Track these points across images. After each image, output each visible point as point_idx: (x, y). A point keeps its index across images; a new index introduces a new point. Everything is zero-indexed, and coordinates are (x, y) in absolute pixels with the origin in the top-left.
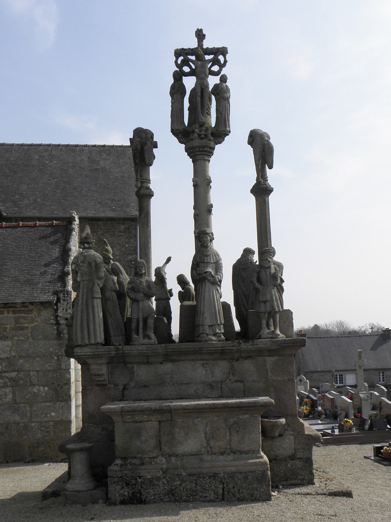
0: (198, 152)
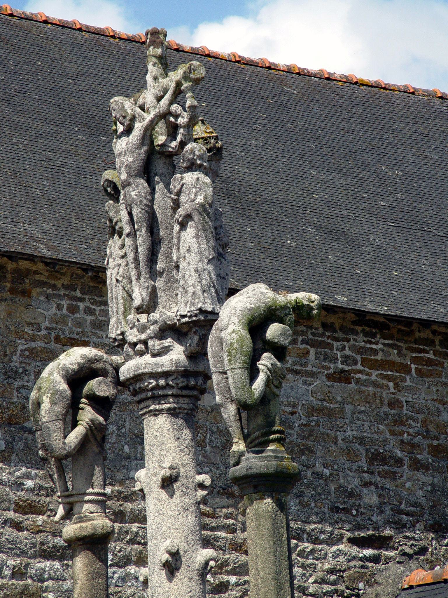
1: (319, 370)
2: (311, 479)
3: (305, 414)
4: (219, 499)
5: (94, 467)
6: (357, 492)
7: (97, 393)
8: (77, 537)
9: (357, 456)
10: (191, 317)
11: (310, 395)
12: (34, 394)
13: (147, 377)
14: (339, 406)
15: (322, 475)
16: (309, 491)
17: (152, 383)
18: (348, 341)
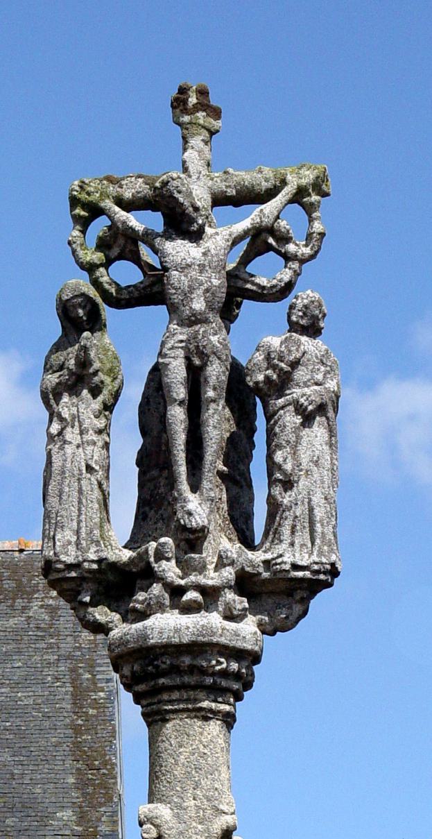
0: (164, 674)
10: (318, 572)
13: (216, 649)
17: (222, 663)
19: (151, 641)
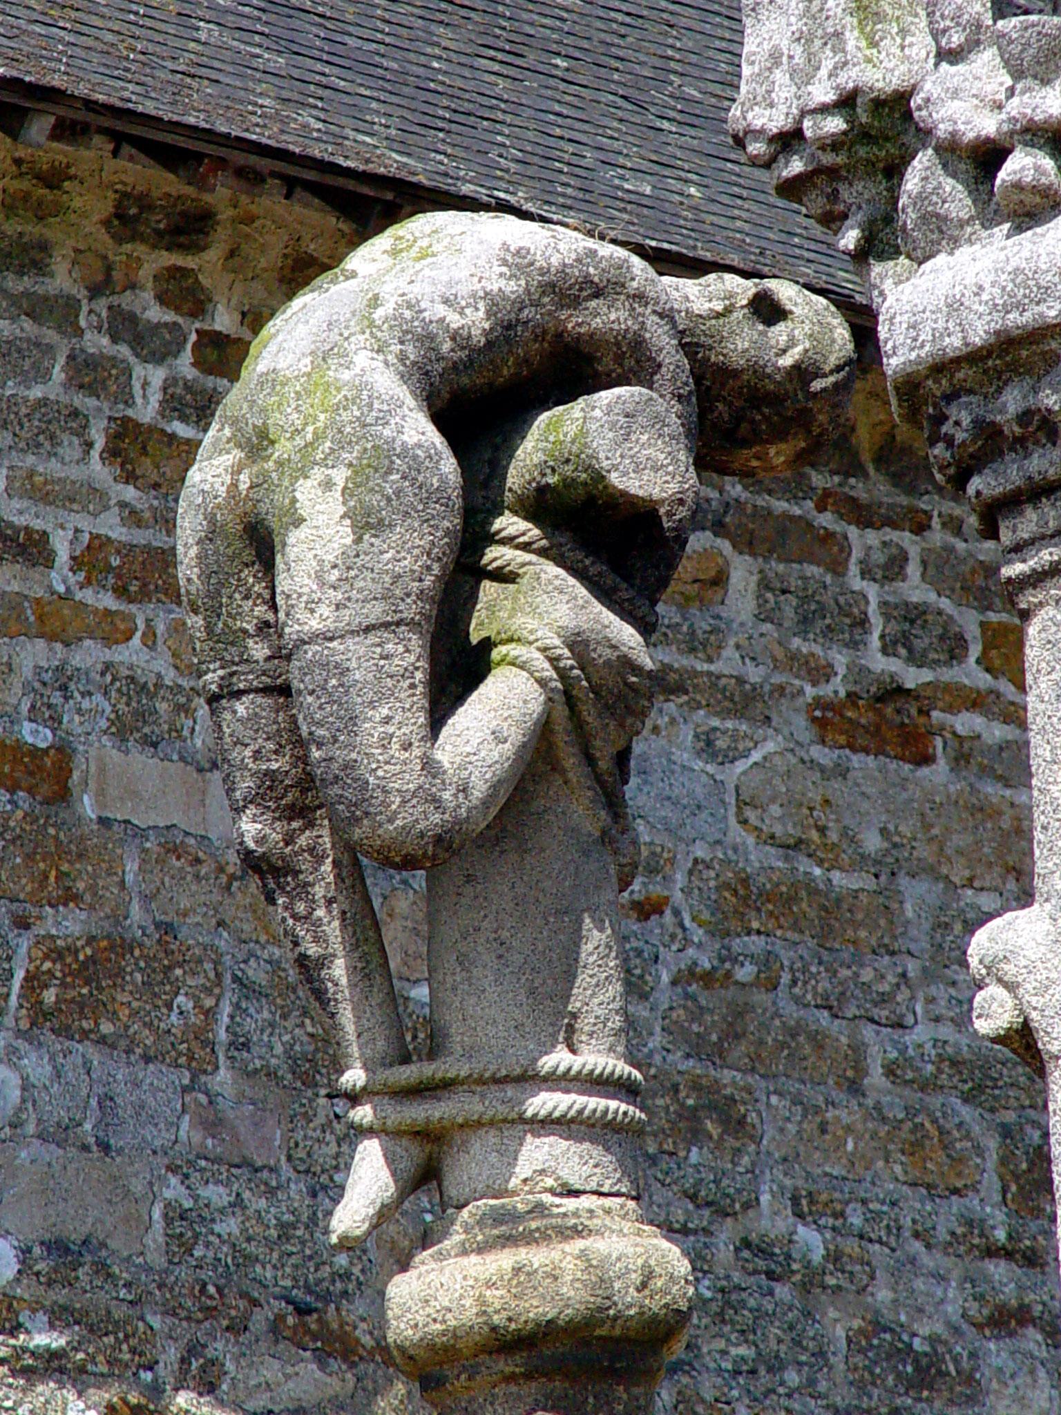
1: (777, 679)
2: (737, 1277)
3: (705, 916)
4: (276, 1364)
5: (580, 922)
6: (956, 1360)
7: (614, 479)
8: (494, 1329)
9: (958, 1161)
11: (733, 810)
12: (212, 473)
14: (871, 884)
15: (788, 1257)
16: (721, 1344)
18: (920, 528)
19: (894, 361)
